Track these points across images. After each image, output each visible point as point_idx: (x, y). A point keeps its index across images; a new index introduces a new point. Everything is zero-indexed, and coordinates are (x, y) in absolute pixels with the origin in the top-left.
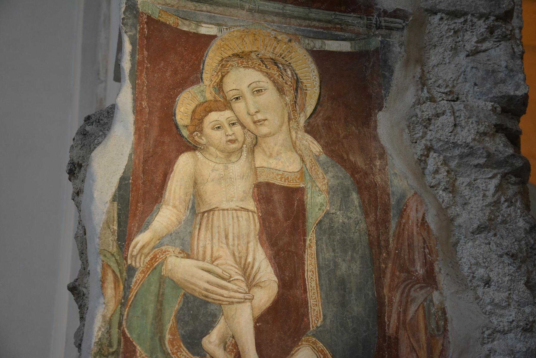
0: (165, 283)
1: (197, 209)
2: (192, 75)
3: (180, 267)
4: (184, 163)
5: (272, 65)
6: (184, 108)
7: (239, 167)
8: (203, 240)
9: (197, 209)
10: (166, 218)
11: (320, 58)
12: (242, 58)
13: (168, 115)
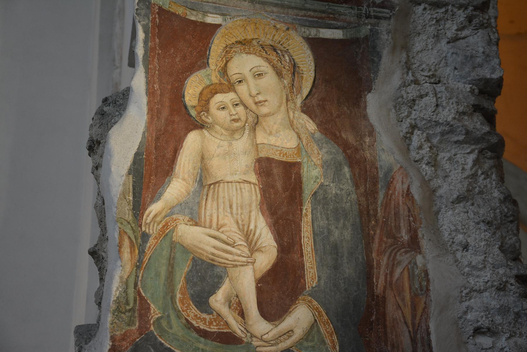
0: (176, 249)
1: (204, 182)
2: (200, 61)
3: (189, 234)
4: (192, 140)
5: (272, 51)
6: (192, 90)
7: (242, 143)
8: (210, 210)
9: (204, 182)
10: (176, 189)
11: (316, 45)
12: (244, 44)
13: (178, 96)
